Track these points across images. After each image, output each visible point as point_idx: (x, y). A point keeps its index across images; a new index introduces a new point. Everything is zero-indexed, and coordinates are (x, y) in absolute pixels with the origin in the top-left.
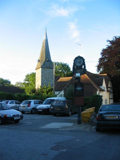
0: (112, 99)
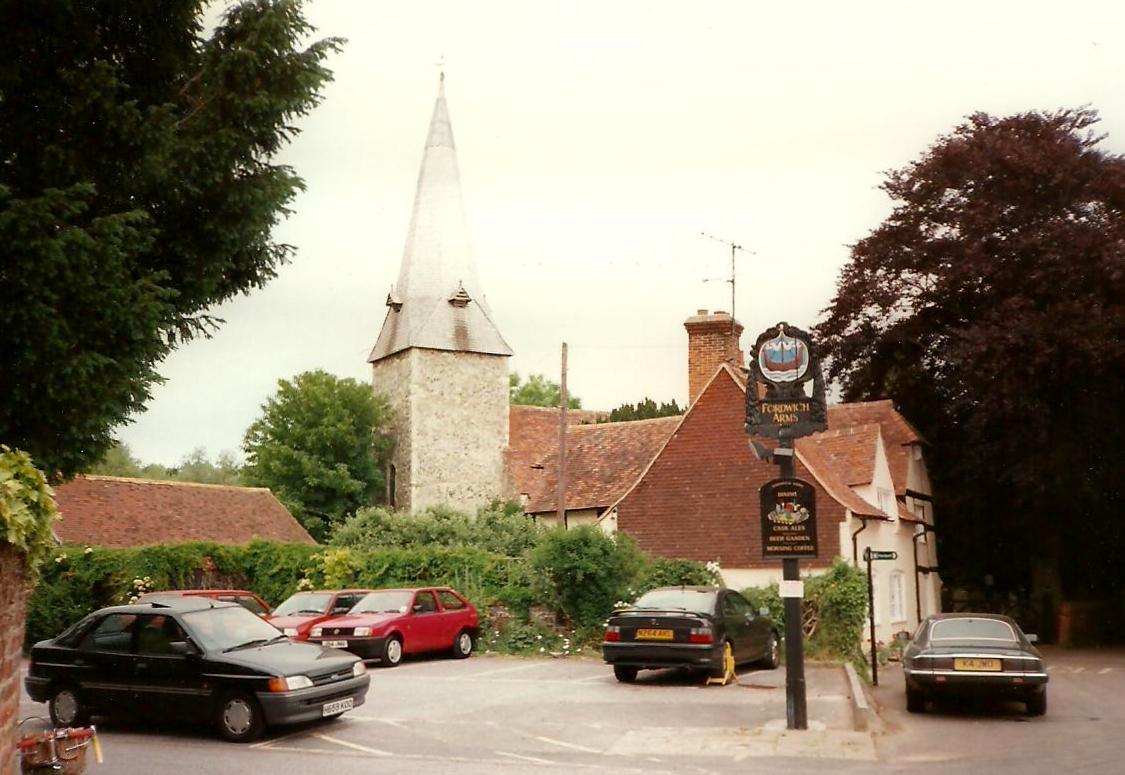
0: (931, 569)
